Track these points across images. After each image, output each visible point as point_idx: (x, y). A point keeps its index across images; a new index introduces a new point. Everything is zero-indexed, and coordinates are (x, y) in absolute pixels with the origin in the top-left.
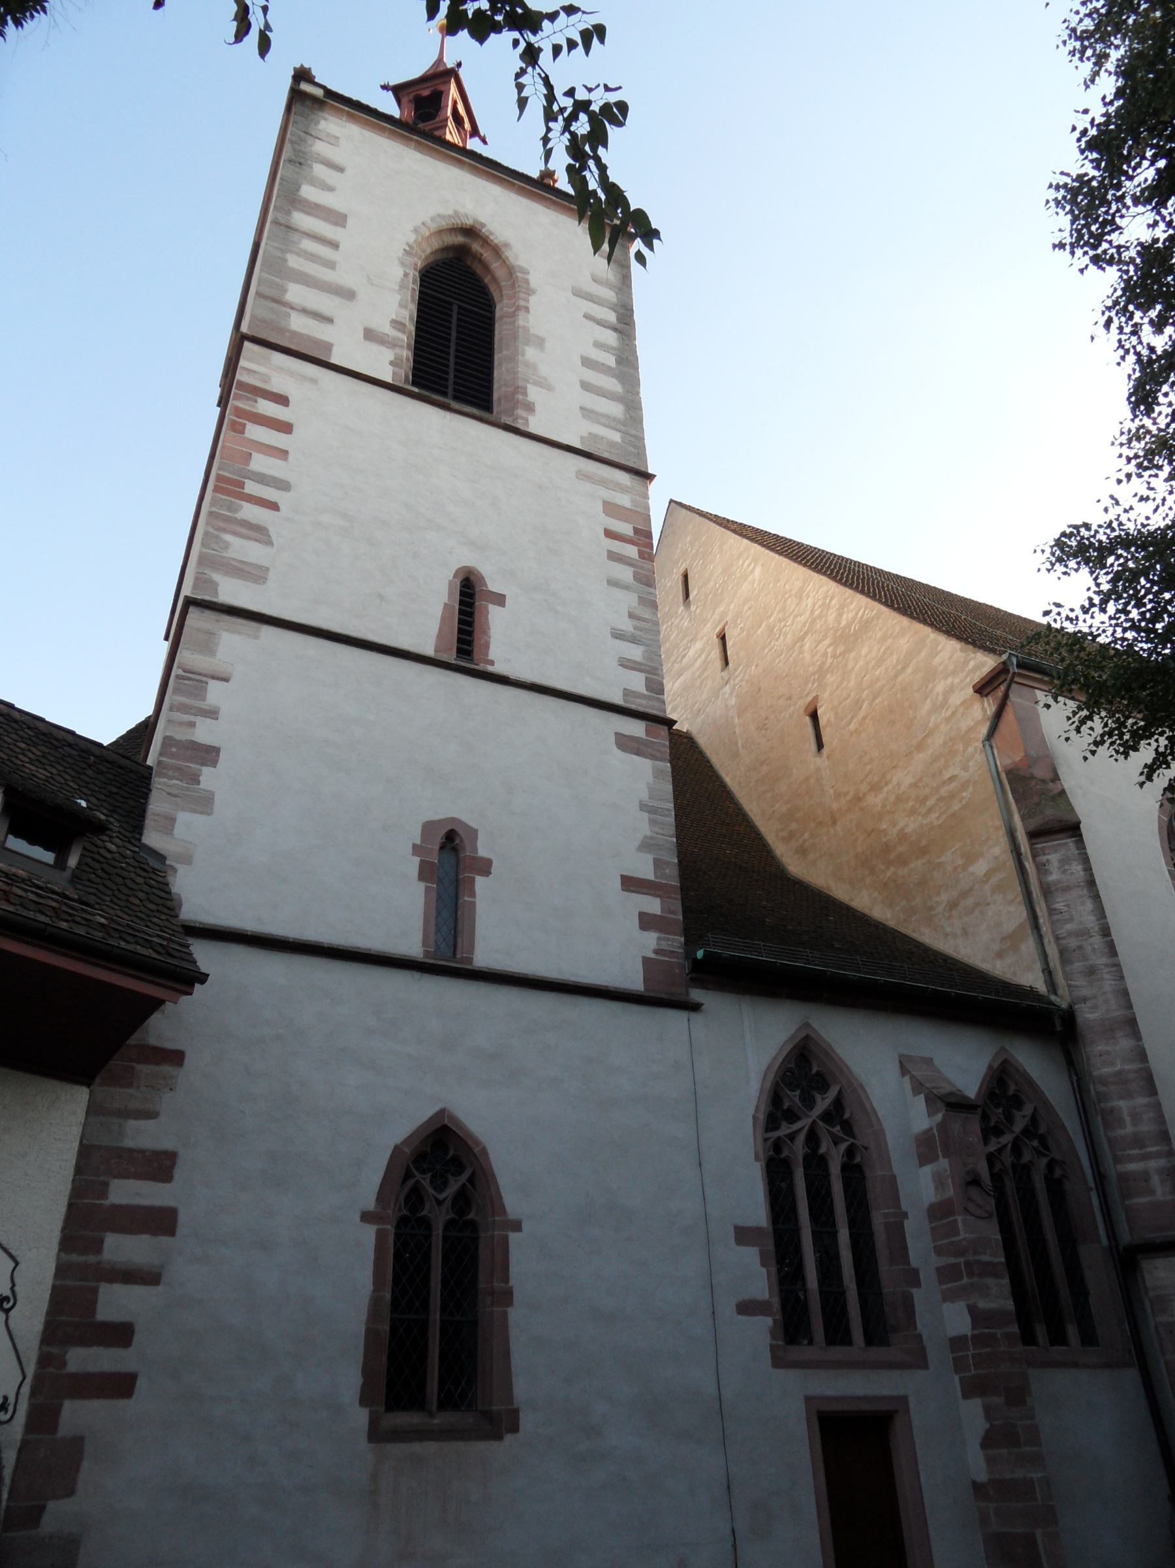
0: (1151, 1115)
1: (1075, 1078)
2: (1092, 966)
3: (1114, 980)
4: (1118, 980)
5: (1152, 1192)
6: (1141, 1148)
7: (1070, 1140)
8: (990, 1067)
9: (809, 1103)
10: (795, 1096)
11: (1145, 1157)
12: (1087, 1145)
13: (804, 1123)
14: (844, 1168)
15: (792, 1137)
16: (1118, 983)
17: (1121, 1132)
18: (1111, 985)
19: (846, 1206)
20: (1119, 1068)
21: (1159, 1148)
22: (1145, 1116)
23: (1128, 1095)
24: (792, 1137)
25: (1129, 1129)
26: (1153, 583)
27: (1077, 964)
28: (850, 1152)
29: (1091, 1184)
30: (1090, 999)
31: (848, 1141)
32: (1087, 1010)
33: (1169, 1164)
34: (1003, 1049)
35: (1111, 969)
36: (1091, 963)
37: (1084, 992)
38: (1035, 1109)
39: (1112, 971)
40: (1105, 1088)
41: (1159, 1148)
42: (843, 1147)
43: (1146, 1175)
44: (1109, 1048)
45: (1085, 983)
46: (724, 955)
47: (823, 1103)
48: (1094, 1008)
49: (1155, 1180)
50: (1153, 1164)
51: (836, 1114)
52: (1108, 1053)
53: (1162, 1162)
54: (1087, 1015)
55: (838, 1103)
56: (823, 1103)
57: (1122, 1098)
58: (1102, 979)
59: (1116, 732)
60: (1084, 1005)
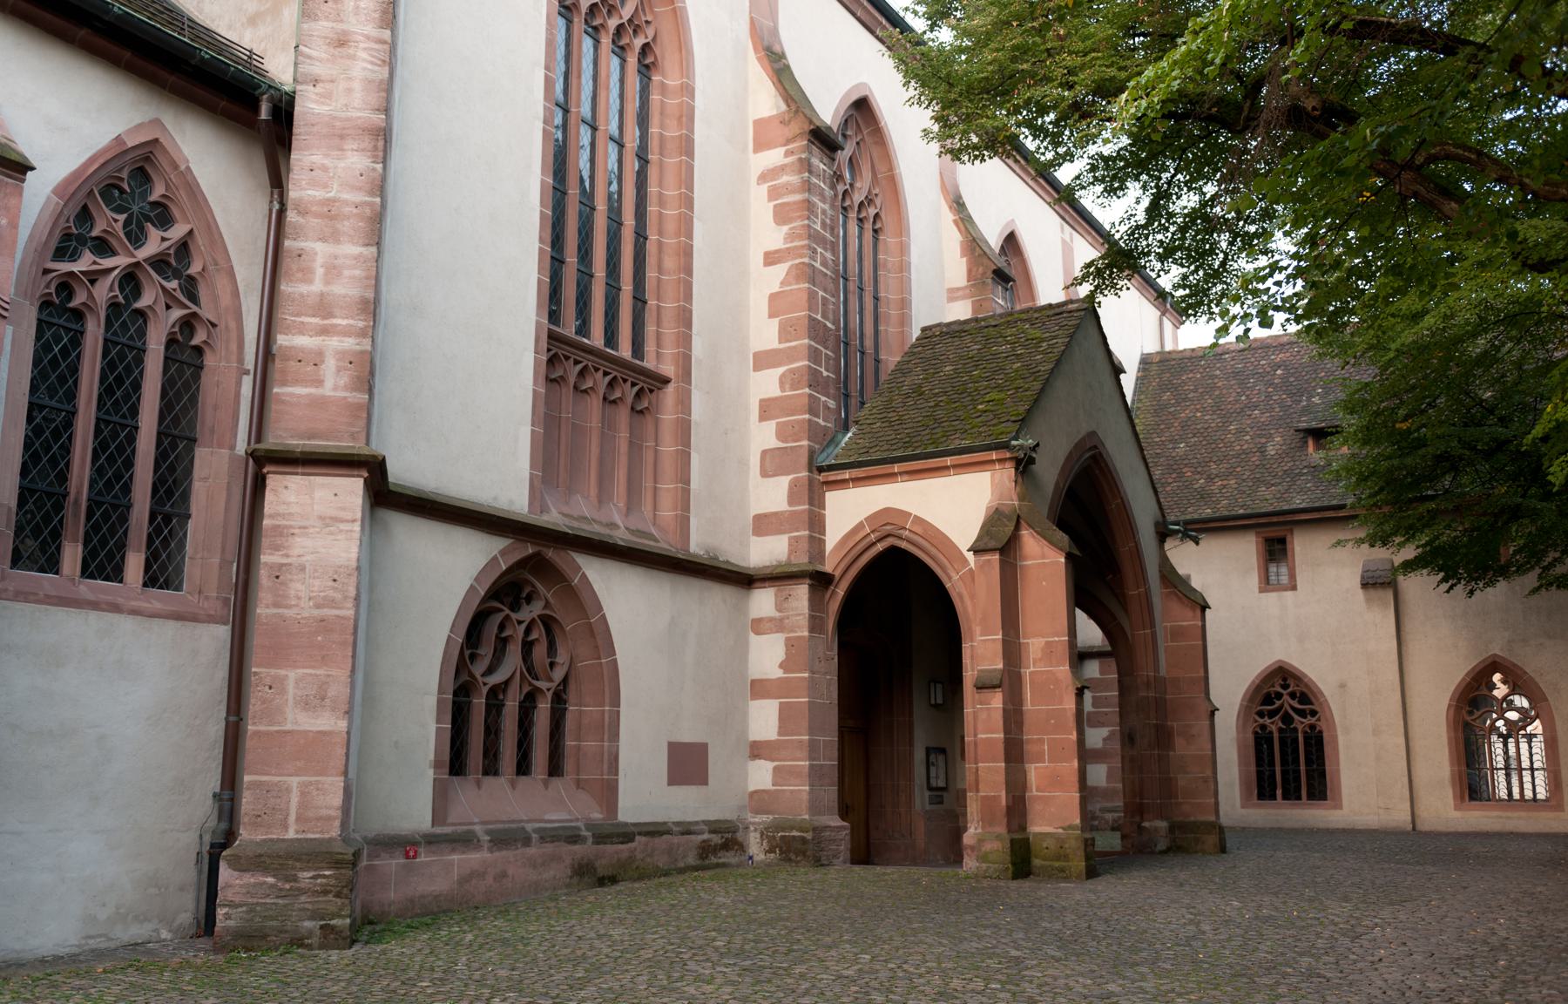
0: (357, 272)
1: (276, 206)
2: (345, 33)
3: (372, 63)
4: (379, 66)
5: (319, 382)
6: (324, 318)
7: (236, 294)
8: (118, 140)
9: (136, 237)
10: (116, 221)
11: (324, 331)
12: (857, 481)
13: (121, 261)
14: (171, 342)
15: (93, 277)
16: (376, 68)
17: (303, 289)
18: (364, 69)
19: (163, 386)
20: (331, 195)
21: (351, 322)
22: (346, 273)
23: (333, 237)
24: (93, 277)
25: (317, 286)
26: (1245, 64)
27: (325, 23)
28: (188, 324)
29: (250, 361)
30: (323, 81)
31: (190, 308)
32: (314, 97)
33: (358, 347)
34: (157, 122)
35: (376, 46)
36: (344, 27)
37: (317, 69)
38: (191, 232)
39: (372, 49)
40: (301, 220)
41: (351, 322)
42: (177, 313)
43: (317, 358)
44: (327, 162)
45: (324, 55)
46: (116, 9)
47: (154, 243)
48: (327, 96)
49: (330, 365)
50: (334, 343)
51: (174, 262)
52: (325, 169)
53: (349, 343)
54: (309, 107)
55: (184, 248)
56: (154, 243)
57: (323, 239)
58: (353, 57)
59: (1300, 312)
60: (311, 88)
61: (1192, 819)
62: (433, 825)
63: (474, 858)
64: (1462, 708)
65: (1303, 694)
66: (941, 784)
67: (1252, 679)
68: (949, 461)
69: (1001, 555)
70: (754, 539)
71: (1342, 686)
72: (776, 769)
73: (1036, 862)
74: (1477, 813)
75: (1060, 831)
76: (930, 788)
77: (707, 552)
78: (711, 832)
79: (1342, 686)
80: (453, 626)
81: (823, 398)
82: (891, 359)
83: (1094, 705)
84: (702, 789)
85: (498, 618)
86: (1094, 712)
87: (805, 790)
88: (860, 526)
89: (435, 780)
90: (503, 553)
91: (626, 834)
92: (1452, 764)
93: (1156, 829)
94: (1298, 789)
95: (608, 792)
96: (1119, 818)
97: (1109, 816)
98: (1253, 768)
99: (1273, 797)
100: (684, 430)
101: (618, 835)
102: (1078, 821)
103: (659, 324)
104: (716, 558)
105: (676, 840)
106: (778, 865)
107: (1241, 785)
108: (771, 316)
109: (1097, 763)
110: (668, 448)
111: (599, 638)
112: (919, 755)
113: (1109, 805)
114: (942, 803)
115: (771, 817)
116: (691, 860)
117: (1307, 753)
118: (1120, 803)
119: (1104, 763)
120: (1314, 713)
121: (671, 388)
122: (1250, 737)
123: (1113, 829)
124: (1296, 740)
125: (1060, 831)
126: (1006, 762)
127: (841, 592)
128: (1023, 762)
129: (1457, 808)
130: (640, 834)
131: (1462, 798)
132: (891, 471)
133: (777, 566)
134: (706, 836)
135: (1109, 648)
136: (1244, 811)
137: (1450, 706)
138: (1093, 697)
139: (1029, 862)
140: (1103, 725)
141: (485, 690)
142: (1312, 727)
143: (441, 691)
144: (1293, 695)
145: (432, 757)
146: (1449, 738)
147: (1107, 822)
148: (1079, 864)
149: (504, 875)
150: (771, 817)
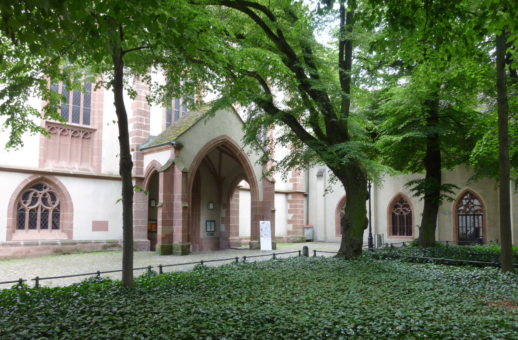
62: (7, 241)
63: (18, 248)
66: (213, 230)
74: (393, 239)
76: (207, 231)
77: (109, 173)
78: (107, 242)
80: (12, 196)
81: (144, 131)
83: (290, 207)
84: (106, 232)
85: (33, 193)
88: (149, 164)
89: (7, 231)
90: (29, 178)
91: (75, 244)
92: (387, 225)
94: (397, 232)
95: (70, 234)
97: (292, 239)
98: (391, 226)
99: (396, 235)
100: (100, 143)
101: (71, 243)
102: (181, 241)
103: (94, 115)
104: (112, 174)
105: (93, 244)
108: (132, 109)
110: (95, 147)
111: (66, 196)
114: (213, 235)
116: (99, 249)
121: (97, 132)
126: (162, 226)
127: (147, 182)
130: (79, 243)
131: (390, 235)
134: (105, 244)
136: (336, 238)
139: (172, 251)
140: (292, 213)
141: (28, 210)
143: (8, 210)
145: (6, 225)
148: (180, 252)
149: (29, 252)
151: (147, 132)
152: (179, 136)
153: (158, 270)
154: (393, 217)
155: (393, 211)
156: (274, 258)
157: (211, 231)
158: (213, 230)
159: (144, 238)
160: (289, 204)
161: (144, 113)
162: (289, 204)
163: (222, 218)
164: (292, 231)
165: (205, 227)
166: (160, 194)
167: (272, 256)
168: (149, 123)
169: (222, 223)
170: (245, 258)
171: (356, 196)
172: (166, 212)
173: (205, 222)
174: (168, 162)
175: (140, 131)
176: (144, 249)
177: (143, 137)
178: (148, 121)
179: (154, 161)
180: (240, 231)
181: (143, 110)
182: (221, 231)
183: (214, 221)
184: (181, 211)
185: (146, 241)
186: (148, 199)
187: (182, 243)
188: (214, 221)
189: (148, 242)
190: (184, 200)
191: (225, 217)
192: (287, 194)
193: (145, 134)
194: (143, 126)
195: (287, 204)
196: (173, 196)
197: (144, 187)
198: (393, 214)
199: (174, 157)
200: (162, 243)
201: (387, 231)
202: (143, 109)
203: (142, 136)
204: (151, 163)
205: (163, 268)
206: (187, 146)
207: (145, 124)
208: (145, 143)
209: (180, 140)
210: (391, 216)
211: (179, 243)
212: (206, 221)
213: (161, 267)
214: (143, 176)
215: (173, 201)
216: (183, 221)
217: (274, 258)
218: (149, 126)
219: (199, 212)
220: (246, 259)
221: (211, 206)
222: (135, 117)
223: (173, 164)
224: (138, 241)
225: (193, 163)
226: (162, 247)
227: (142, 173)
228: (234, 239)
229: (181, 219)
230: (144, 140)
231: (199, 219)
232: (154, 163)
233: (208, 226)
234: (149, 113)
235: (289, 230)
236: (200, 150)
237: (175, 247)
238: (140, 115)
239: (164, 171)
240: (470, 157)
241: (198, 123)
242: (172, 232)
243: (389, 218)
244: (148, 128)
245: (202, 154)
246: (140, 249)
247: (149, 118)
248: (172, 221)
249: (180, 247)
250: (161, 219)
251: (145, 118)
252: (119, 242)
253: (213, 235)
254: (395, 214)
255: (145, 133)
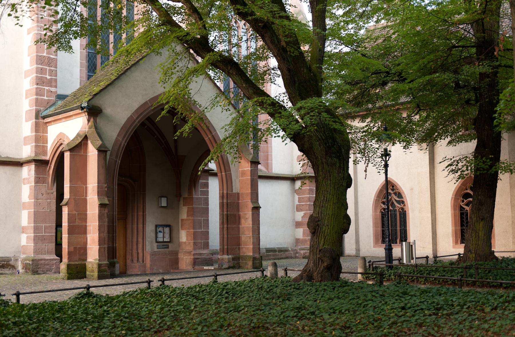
61: (246, 254)
64: (458, 199)
65: (399, 193)
66: (167, 239)
67: (378, 187)
68: (71, 113)
69: (70, 152)
70: (24, 147)
71: (412, 189)
72: (27, 237)
73: (88, 273)
75: (94, 261)
76: (157, 242)
79: (412, 189)
82: (312, 34)
83: (299, 202)
86: (299, 205)
87: (32, 245)
92: (373, 228)
93: (223, 259)
94: (396, 239)
96: (306, 253)
98: (459, 228)
102: (98, 257)
106: (24, 274)
107: (373, 237)
108: (29, 56)
109: (299, 228)
112: (150, 228)
113: (303, 247)
114: (168, 248)
115: (26, 255)
117: (396, 219)
118: (308, 246)
119: (302, 228)
120: (403, 202)
122: (379, 214)
123: (304, 258)
124: (395, 215)
125: (94, 261)
127: (52, 167)
128: (86, 234)
129: (454, 247)
131: (456, 243)
132: (70, 115)
133: (28, 157)
135: (313, 175)
136: (374, 248)
137: (452, 198)
138: (299, 198)
140: (302, 210)
142: (402, 209)
144: (395, 193)
146: (452, 213)
147: (301, 254)
148: (96, 274)
150: (26, 255)
151: (53, 89)
152: (95, 95)
153: (14, 299)
154: (462, 214)
155: (462, 204)
156: (215, 282)
157: (164, 242)
158: (167, 239)
159: (49, 253)
160: (297, 197)
161: (46, 61)
162: (297, 197)
163: (182, 220)
164: (302, 240)
165: (153, 235)
166: (65, 186)
167: (211, 279)
168: (56, 76)
169: (182, 229)
170: (163, 281)
171: (329, 182)
172: (74, 212)
173: (153, 228)
174: (78, 135)
175: (40, 89)
176: (49, 271)
177: (45, 98)
178: (53, 73)
179: (61, 134)
180: (210, 241)
181: (44, 56)
182: (181, 240)
183: (169, 226)
184: (96, 211)
185: (52, 258)
186: (55, 193)
187: (99, 260)
188: (169, 226)
189: (56, 259)
190: (100, 193)
191: (186, 220)
192: (292, 179)
193: (50, 93)
194: (45, 80)
195: (294, 196)
196: (86, 187)
197: (49, 174)
198: (461, 208)
199: (87, 127)
200: (69, 261)
201: (453, 236)
202: (45, 54)
203: (44, 96)
204: (57, 137)
205: (21, 296)
206: (108, 110)
207: (49, 77)
208: (50, 107)
209: (98, 102)
210: (458, 212)
211: (95, 260)
212: (156, 226)
213: (18, 295)
214: (47, 158)
215: (86, 196)
216: (100, 226)
217: (215, 282)
218: (56, 80)
219: (144, 211)
220: (165, 282)
221: (164, 203)
222: (33, 67)
223: (86, 138)
224: (39, 258)
225: (119, 135)
226: (69, 266)
227: (45, 153)
228: (200, 254)
229: (97, 224)
230: (48, 102)
231: (144, 224)
232: (61, 136)
233: (160, 235)
234: (56, 60)
235: (297, 237)
236: (131, 116)
237: (89, 266)
238: (41, 64)
239: (71, 150)
240: (495, 118)
241: (127, 73)
242: (86, 243)
243: (454, 216)
244: (54, 84)
245: (135, 121)
246: (43, 271)
247: (56, 68)
248: (86, 226)
249: (96, 267)
250: (67, 224)
251: (48, 68)
252: (11, 260)
253: (168, 248)
254: (464, 209)
255: (49, 91)
